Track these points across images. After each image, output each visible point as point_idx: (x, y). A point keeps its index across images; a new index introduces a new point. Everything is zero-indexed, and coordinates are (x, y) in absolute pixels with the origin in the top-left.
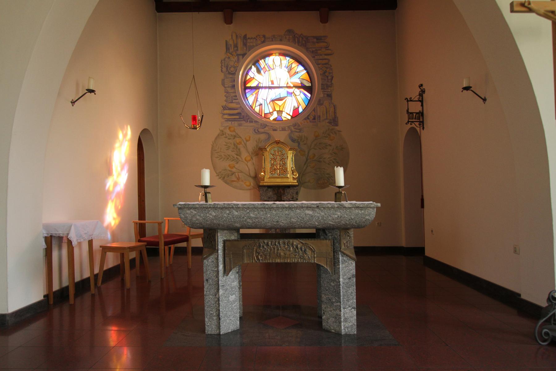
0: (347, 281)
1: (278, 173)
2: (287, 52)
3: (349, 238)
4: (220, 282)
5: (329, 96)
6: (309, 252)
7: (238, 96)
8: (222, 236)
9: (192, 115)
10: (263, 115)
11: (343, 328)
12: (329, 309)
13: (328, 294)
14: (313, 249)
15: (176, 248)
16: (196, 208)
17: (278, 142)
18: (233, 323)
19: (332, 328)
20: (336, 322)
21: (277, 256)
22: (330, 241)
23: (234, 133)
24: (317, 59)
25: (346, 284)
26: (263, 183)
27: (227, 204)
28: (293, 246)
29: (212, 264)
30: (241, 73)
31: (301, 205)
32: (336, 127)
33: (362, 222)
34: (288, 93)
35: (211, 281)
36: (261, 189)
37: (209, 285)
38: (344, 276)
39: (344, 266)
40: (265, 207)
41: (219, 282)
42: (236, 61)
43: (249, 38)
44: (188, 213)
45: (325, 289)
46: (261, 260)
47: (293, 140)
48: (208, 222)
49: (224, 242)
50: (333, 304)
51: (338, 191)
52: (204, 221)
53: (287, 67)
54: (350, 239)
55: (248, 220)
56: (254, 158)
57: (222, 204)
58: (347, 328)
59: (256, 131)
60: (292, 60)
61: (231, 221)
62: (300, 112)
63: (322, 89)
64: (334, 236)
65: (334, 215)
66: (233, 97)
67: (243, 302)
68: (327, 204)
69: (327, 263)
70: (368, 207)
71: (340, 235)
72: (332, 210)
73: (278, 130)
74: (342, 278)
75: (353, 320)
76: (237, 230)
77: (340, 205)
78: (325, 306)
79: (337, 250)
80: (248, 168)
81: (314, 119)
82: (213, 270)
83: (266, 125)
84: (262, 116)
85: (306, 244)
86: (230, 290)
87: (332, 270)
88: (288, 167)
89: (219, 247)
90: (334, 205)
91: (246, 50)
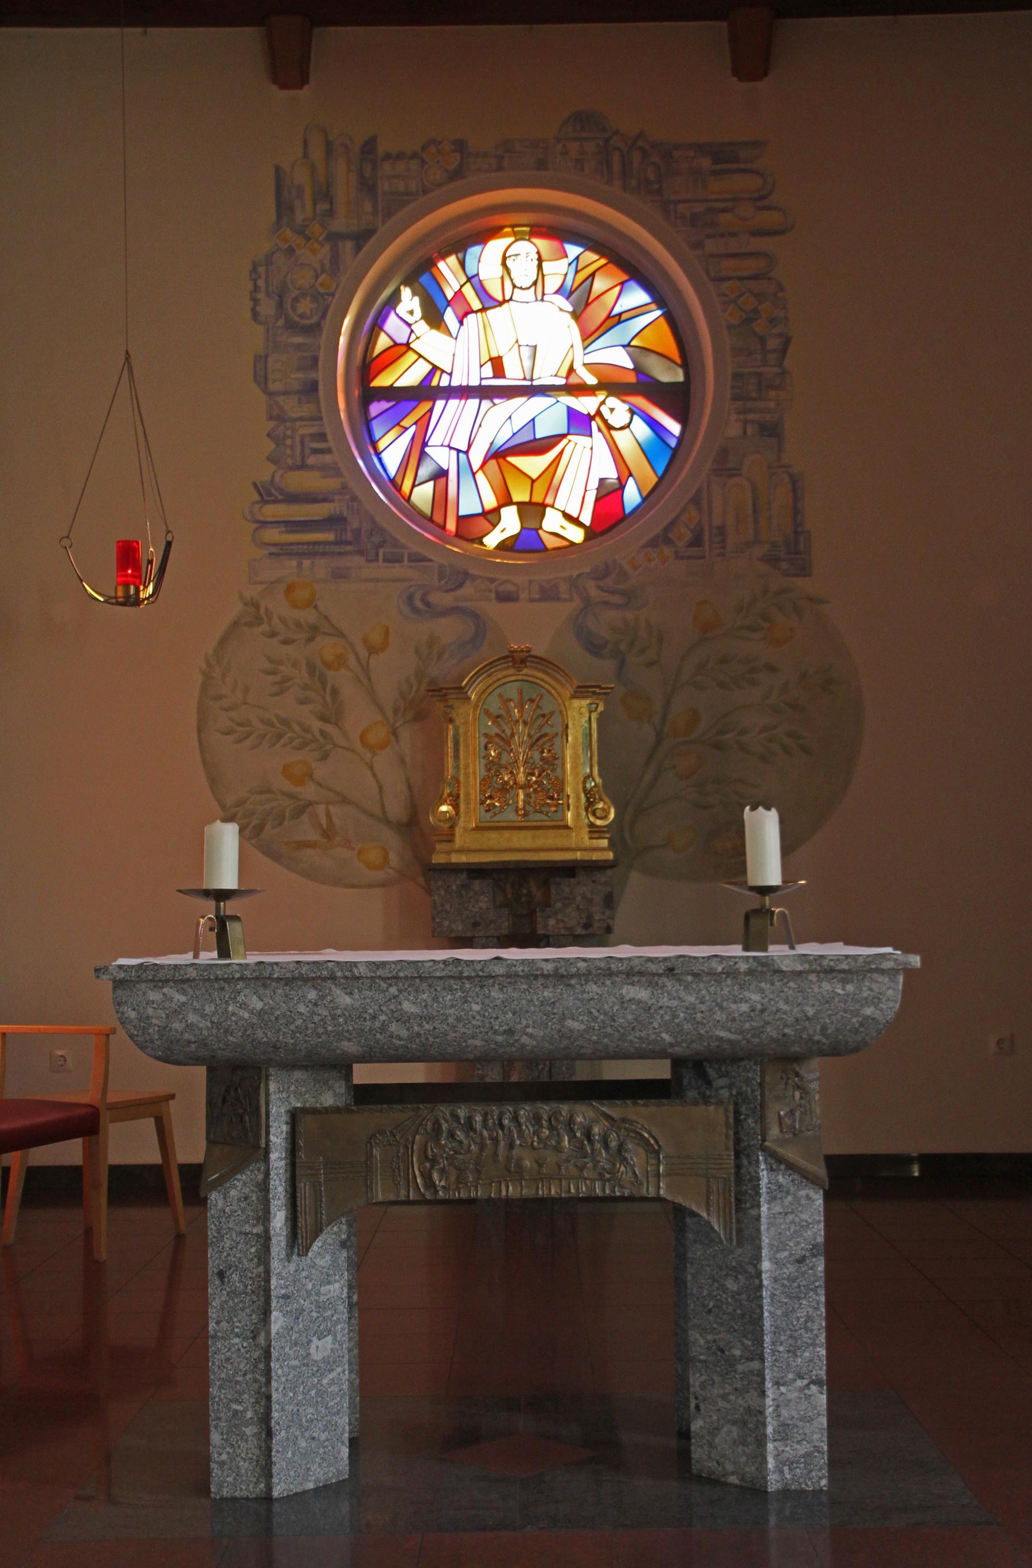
0: (790, 1269)
1: (521, 804)
2: (570, 222)
3: (801, 1098)
4: (274, 1281)
5: (771, 431)
6: (637, 1156)
7: (330, 437)
8: (284, 1095)
9: (118, 542)
10: (451, 525)
11: (771, 1463)
12: (716, 1391)
13: (715, 1326)
14: (652, 1142)
15: (35, 1175)
16: (183, 981)
17: (520, 660)
18: (321, 1451)
19: (730, 1467)
20: (744, 1443)
21: (509, 1171)
22: (721, 1109)
23: (309, 616)
24: (712, 256)
25: (786, 1282)
26: (449, 853)
27: (308, 963)
28: (572, 1133)
29: (243, 1210)
30: (347, 322)
31: (602, 965)
32: (800, 582)
33: (850, 1031)
34: (572, 414)
35: (235, 1277)
36: (440, 883)
37: (228, 1295)
38: (778, 1251)
39: (778, 1209)
40: (461, 972)
41: (269, 1281)
42: (323, 265)
43: (388, 156)
44: (153, 1002)
45: (704, 1306)
46: (443, 1187)
47: (595, 647)
48: (231, 1039)
49: (294, 1117)
50: (733, 1365)
51: (758, 906)
52: (214, 1031)
53: (571, 293)
54: (803, 1102)
55: (393, 1027)
56: (405, 734)
57: (288, 963)
58: (791, 1463)
59: (418, 604)
60: (595, 257)
61: (326, 1032)
62: (628, 510)
63: (735, 398)
64: (740, 1088)
65: (735, 1002)
66: (307, 439)
67: (361, 1374)
68: (709, 958)
69: (708, 1198)
70: (871, 971)
71: (761, 1085)
72: (729, 982)
73: (524, 595)
74: (770, 1259)
75: (813, 1432)
76: (343, 1067)
77: (763, 965)
78: (703, 1378)
79: (749, 1145)
80: (377, 781)
81: (697, 541)
82: (246, 1234)
83: (466, 574)
84: (443, 527)
85: (623, 1120)
86: (314, 1314)
87: (731, 1228)
88: (569, 778)
89: (272, 1138)
90: (736, 963)
91: (375, 213)
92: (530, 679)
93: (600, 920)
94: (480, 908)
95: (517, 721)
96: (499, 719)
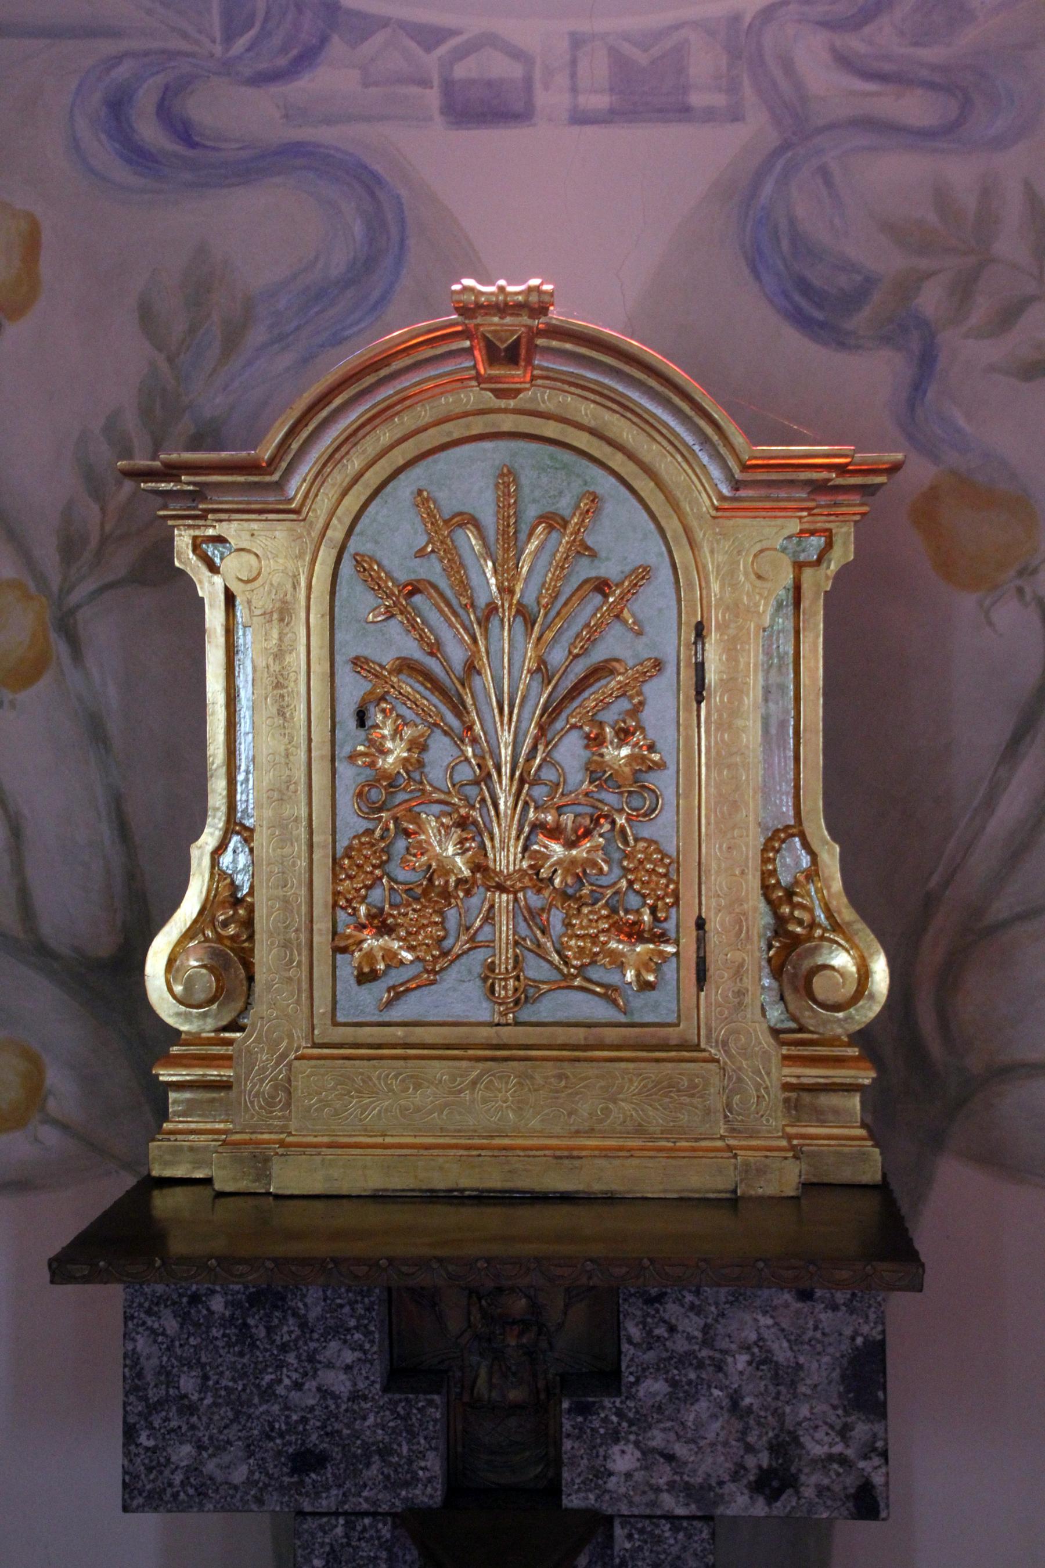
92: (551, 429)
93: (831, 1458)
94: (324, 1392)
95: (492, 609)
96: (417, 599)
